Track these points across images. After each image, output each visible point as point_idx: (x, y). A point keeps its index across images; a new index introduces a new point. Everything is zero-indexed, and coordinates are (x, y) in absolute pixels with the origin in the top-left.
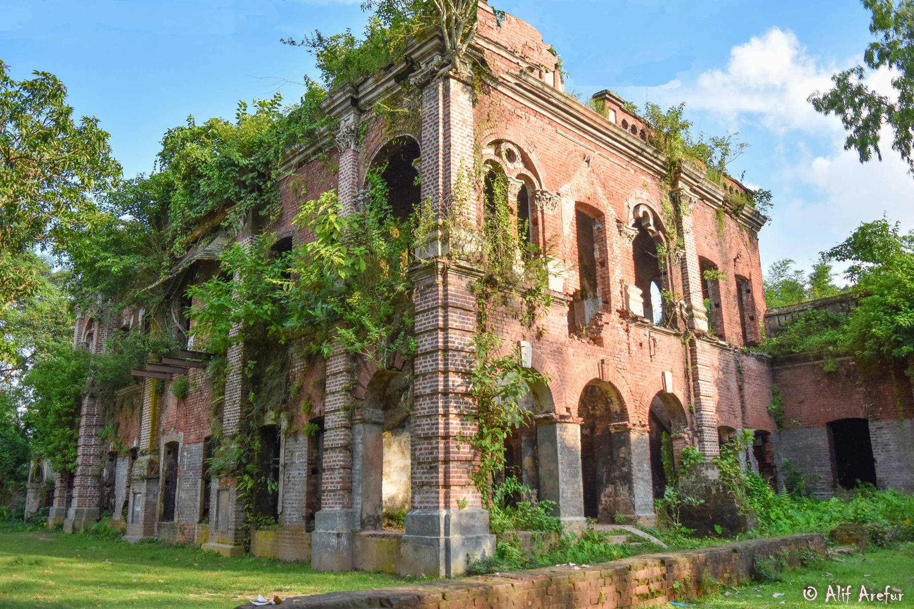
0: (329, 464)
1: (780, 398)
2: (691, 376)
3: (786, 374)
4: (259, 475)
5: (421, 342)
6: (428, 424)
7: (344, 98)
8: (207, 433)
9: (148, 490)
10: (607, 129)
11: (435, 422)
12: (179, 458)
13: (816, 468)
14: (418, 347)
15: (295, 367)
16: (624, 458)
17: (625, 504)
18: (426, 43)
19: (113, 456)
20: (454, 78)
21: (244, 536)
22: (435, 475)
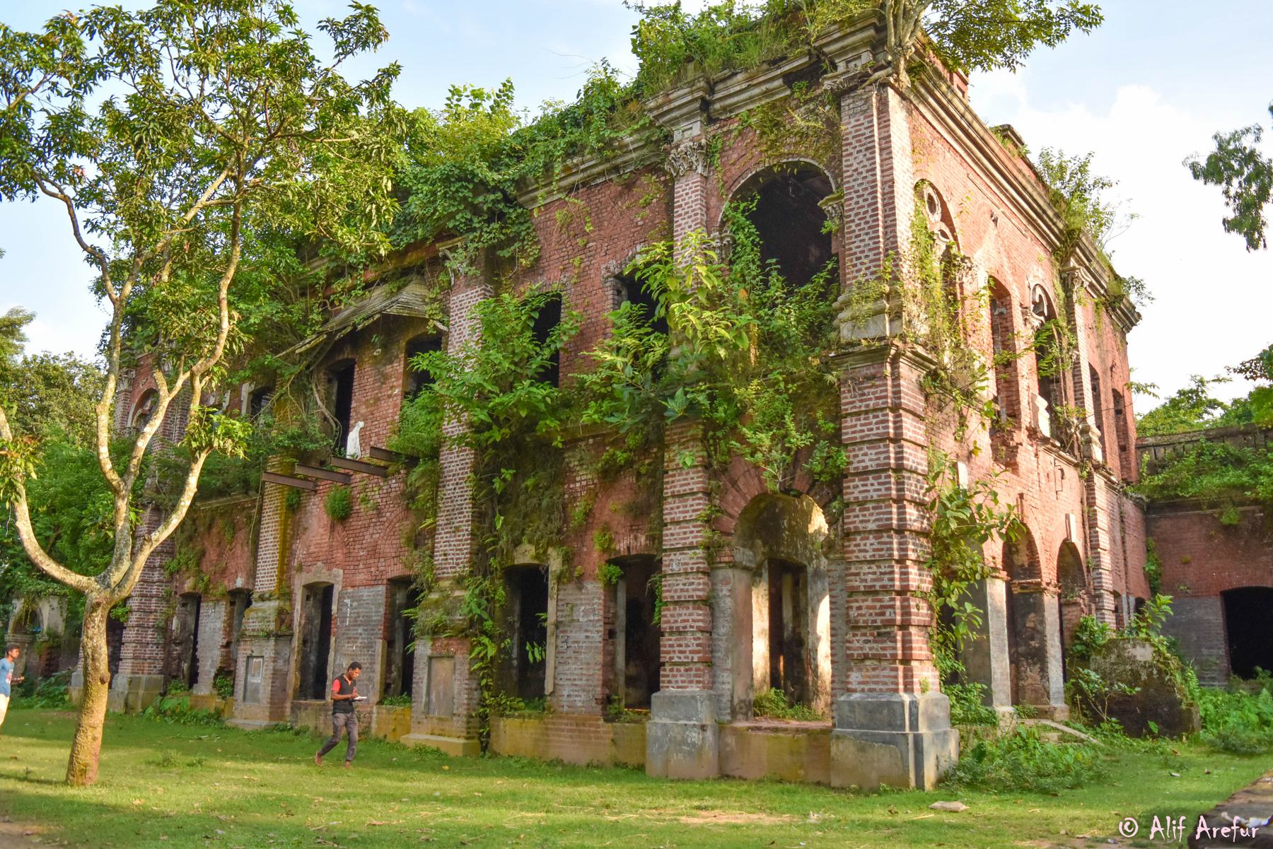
0: (675, 625)
1: (1156, 556)
2: (1089, 522)
3: (1165, 525)
4: (502, 637)
5: (856, 456)
6: (874, 573)
7: (690, 98)
8: (396, 571)
9: (277, 653)
10: (1016, 179)
11: (888, 570)
12: (334, 608)
13: (1205, 651)
14: (849, 463)
15: (575, 482)
16: (1034, 629)
17: (1035, 691)
18: (852, 34)
19: (194, 600)
20: (893, 87)
21: (478, 725)
22: (890, 644)
